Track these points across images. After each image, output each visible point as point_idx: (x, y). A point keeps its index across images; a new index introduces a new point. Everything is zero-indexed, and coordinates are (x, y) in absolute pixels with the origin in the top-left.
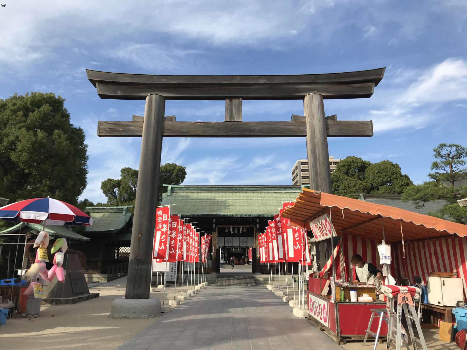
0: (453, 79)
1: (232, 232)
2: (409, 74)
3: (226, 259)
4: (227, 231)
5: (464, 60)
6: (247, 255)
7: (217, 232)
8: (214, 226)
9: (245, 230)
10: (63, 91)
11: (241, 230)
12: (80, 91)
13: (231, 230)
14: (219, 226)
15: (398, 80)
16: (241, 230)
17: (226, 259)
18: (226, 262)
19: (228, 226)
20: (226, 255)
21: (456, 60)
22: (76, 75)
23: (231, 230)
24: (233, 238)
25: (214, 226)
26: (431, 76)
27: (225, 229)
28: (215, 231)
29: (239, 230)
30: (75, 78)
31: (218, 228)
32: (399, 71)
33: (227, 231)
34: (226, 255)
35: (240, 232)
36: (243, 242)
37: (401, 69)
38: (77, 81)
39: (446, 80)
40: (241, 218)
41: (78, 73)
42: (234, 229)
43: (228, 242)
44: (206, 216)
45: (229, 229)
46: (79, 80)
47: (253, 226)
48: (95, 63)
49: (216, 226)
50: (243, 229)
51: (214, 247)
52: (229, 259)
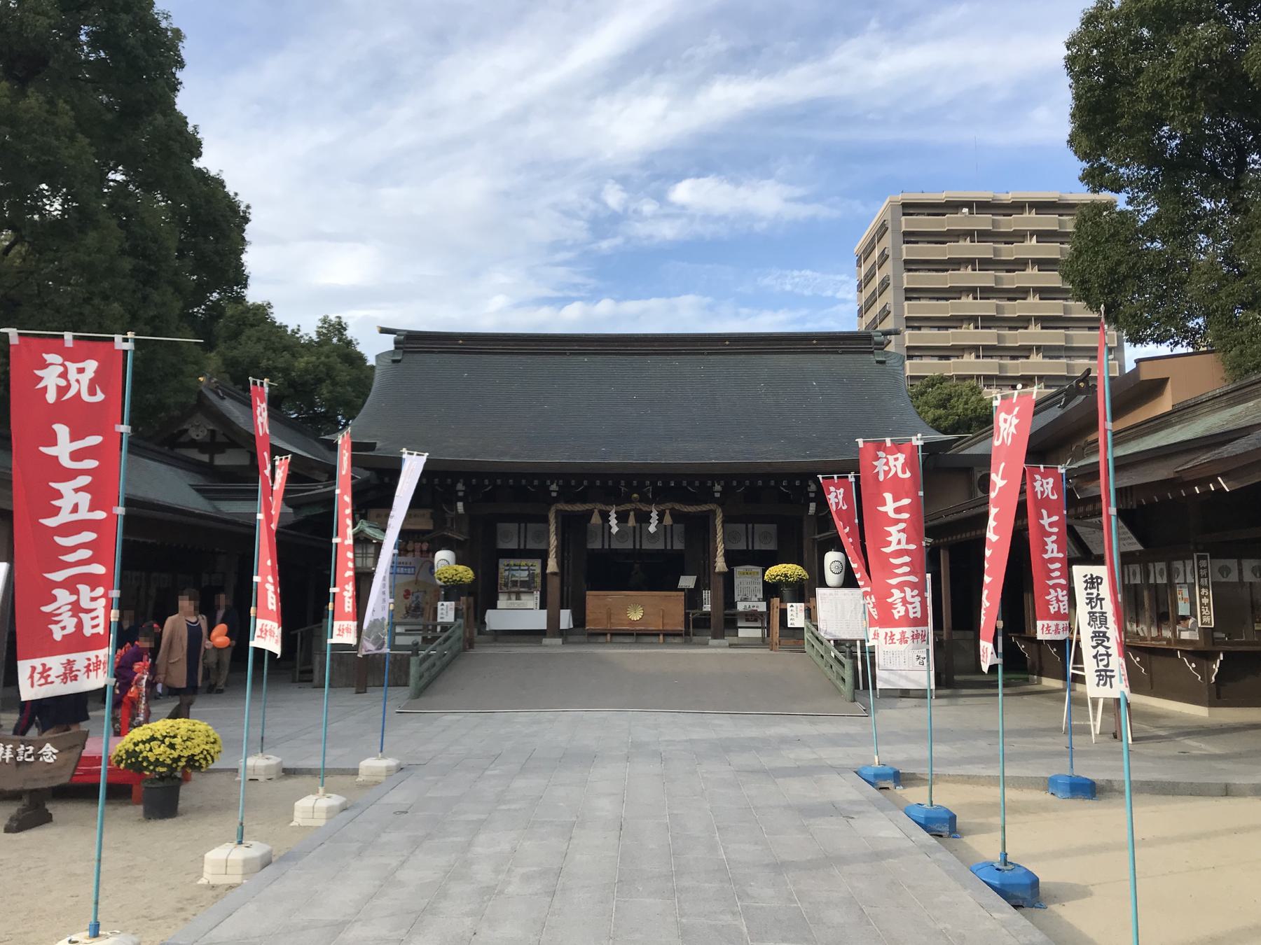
20: (552, 566)
34: (552, 566)
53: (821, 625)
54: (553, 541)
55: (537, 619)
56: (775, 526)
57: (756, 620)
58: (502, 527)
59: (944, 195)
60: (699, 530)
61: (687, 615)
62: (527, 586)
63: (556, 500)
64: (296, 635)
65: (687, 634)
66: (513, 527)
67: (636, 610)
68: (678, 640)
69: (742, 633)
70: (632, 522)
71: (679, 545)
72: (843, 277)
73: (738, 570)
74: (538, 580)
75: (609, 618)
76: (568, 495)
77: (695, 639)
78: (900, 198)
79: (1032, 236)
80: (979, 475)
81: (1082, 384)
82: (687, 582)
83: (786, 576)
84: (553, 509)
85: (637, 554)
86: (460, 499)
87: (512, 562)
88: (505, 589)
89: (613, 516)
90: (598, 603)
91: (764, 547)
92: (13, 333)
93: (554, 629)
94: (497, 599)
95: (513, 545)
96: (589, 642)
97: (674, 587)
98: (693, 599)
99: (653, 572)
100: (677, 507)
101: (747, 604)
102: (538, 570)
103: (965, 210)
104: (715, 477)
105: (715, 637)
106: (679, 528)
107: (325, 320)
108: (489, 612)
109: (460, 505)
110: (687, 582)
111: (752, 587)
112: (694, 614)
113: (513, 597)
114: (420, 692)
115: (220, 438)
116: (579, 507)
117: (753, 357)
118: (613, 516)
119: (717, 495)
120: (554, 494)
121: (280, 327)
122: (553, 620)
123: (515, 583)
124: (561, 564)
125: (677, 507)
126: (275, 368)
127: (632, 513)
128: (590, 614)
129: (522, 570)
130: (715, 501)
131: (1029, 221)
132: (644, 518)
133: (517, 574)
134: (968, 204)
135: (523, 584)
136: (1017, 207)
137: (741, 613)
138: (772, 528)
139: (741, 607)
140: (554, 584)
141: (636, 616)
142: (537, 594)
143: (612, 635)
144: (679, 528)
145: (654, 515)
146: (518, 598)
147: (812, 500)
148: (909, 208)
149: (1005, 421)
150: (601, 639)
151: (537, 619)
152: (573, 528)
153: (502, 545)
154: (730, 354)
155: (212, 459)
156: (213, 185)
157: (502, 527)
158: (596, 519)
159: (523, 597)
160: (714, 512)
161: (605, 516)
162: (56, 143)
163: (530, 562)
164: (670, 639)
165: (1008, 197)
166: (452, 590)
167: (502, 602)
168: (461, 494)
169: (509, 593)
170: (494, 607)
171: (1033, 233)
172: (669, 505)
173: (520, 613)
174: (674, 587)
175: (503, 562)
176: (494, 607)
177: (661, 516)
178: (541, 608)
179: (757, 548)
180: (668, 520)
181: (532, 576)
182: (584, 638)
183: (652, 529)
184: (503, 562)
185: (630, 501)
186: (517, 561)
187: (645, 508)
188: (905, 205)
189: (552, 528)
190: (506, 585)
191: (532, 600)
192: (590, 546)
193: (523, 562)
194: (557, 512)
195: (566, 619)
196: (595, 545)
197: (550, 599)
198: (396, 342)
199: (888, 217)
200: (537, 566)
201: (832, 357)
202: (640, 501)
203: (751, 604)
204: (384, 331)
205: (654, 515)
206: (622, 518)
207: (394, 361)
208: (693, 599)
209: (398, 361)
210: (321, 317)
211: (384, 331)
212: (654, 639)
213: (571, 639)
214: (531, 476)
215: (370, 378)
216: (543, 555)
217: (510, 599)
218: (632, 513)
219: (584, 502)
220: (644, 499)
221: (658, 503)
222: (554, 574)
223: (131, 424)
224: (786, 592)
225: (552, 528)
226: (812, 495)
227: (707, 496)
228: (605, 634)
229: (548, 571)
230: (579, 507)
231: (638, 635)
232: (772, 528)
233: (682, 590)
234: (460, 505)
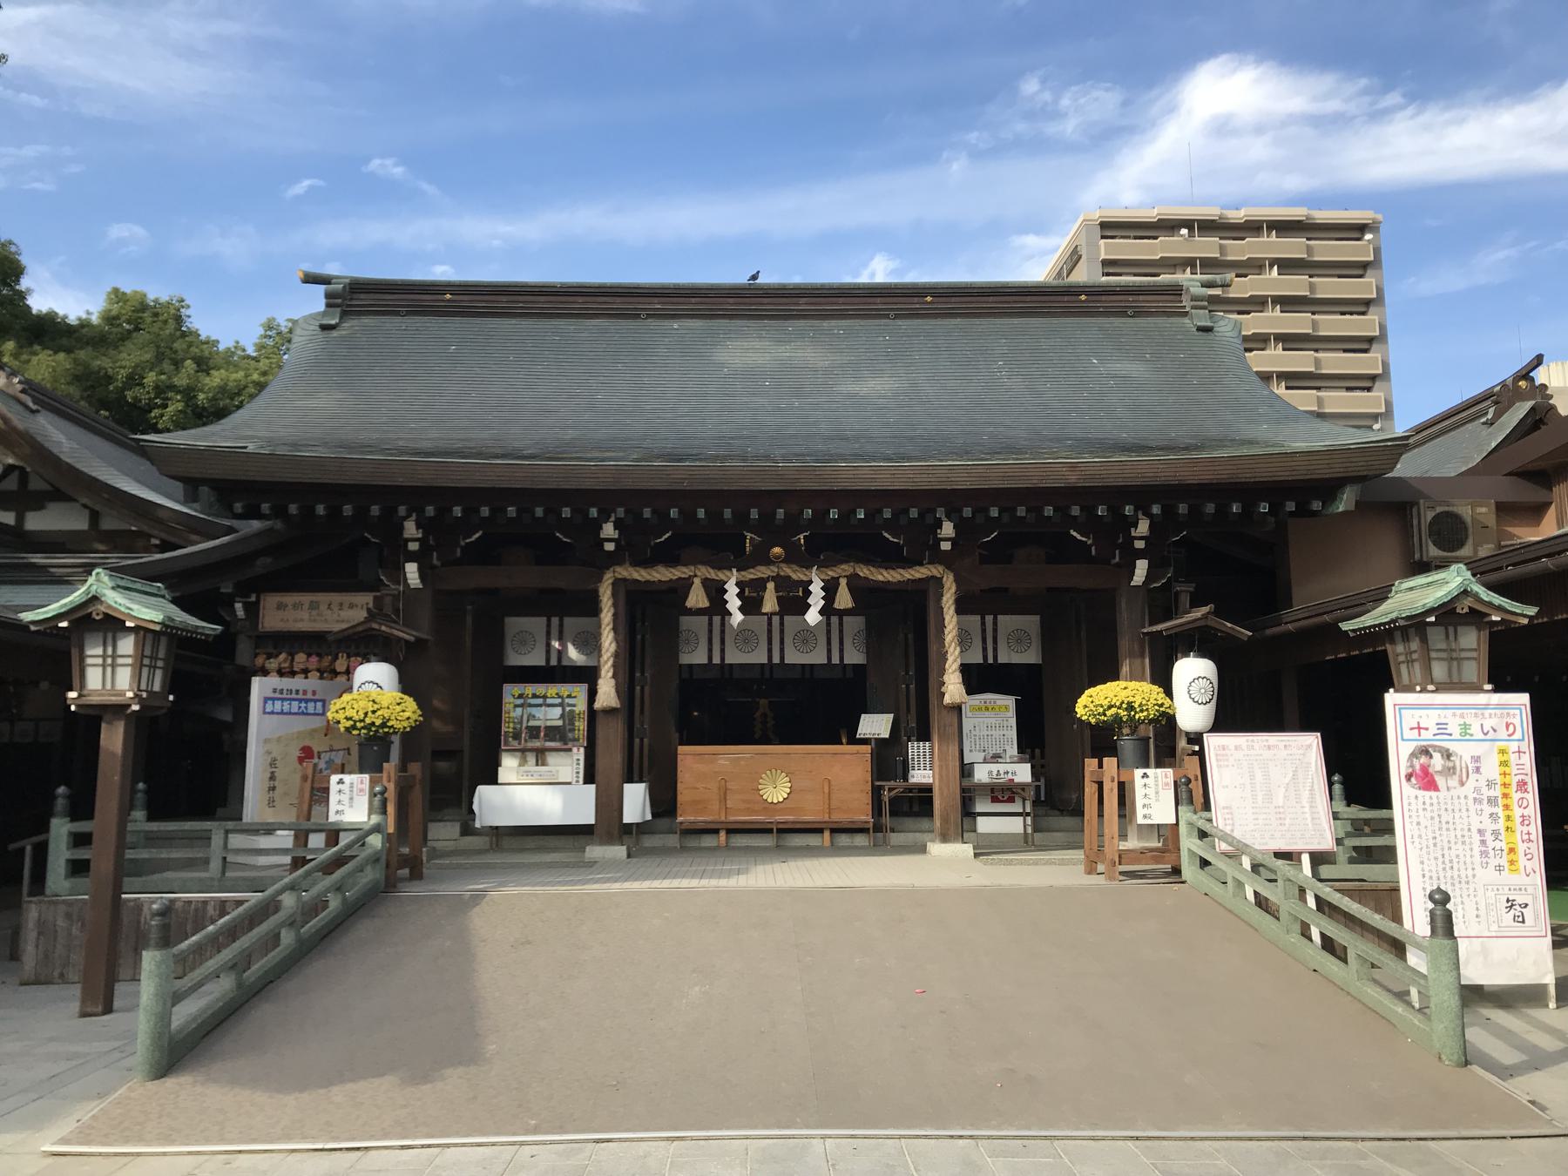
20: (607, 693)
53: (1220, 818)
54: (608, 642)
55: (579, 806)
56: (1037, 618)
57: (1011, 800)
58: (515, 624)
59: (1156, 212)
60: (899, 623)
61: (876, 792)
62: (559, 736)
63: (614, 559)
64: (23, 850)
65: (878, 828)
66: (536, 624)
67: (777, 778)
68: (860, 840)
69: (985, 825)
70: (770, 603)
73: (1485, 634)
74: (581, 725)
75: (724, 799)
76: (635, 549)
77: (896, 839)
78: (1097, 215)
79: (1271, 266)
80: (1430, 515)
81: (1522, 384)
82: (875, 725)
83: (1130, 707)
84: (608, 578)
85: (771, 678)
86: (412, 557)
87: (530, 689)
88: (515, 744)
89: (732, 592)
90: (705, 769)
91: (1017, 659)
93: (608, 825)
94: (497, 764)
95: (535, 659)
96: (683, 849)
98: (888, 759)
99: (805, 709)
100: (864, 571)
101: (994, 767)
102: (581, 705)
103: (1184, 231)
105: (945, 838)
107: (269, 326)
108: (482, 790)
109: (412, 569)
110: (875, 725)
111: (997, 733)
112: (891, 789)
113: (531, 758)
114: (176, 1054)
115: (36, 484)
116: (662, 574)
117: (977, 321)
118: (732, 592)
119: (946, 546)
120: (610, 547)
121: (207, 343)
122: (609, 805)
123: (534, 732)
124: (627, 689)
125: (864, 571)
126: (172, 387)
127: (771, 586)
128: (684, 795)
129: (551, 706)
130: (938, 557)
131: (1270, 245)
132: (795, 603)
133: (539, 713)
134: (1188, 224)
135: (553, 733)
136: (1253, 227)
137: (983, 786)
138: (1031, 622)
139: (982, 774)
140: (612, 736)
141: (776, 791)
142: (579, 754)
143: (730, 831)
145: (816, 588)
146: (541, 761)
147: (1141, 554)
148: (1110, 228)
150: (708, 841)
151: (579, 806)
152: (652, 618)
153: (515, 659)
154: (936, 316)
155: (20, 519)
157: (515, 624)
159: (552, 758)
160: (938, 581)
162: (241, 374)
163: (565, 689)
164: (844, 840)
165: (1238, 215)
166: (370, 748)
167: (509, 766)
168: (413, 546)
169: (523, 751)
170: (493, 780)
171: (1273, 262)
172: (847, 569)
173: (533, 791)
175: (511, 691)
176: (493, 780)
177: (830, 589)
178: (586, 782)
179: (1002, 660)
180: (844, 600)
181: (569, 717)
182: (673, 840)
183: (813, 617)
184: (511, 691)
185: (768, 562)
186: (540, 689)
187: (797, 574)
188: (1104, 225)
189: (607, 616)
190: (517, 736)
191: (568, 766)
192: (686, 659)
193: (552, 690)
194: (617, 583)
195: (635, 802)
196: (695, 656)
197: (601, 763)
198: (328, 296)
199: (1082, 242)
200: (580, 691)
201: (1117, 321)
202: (788, 560)
203: (1002, 767)
204: (311, 279)
205: (816, 588)
207: (324, 328)
208: (888, 759)
209: (332, 327)
210: (264, 320)
211: (311, 279)
212: (813, 840)
213: (649, 841)
215: (680, 730)
216: (588, 676)
217: (523, 762)
218: (771, 586)
219: (673, 561)
221: (823, 565)
222: (609, 712)
224: (1127, 744)
225: (607, 616)
226: (1140, 544)
227: (925, 549)
228: (716, 831)
229: (597, 705)
230: (662, 574)
231: (783, 834)
232: (1031, 622)
233: (865, 741)
234: (412, 569)
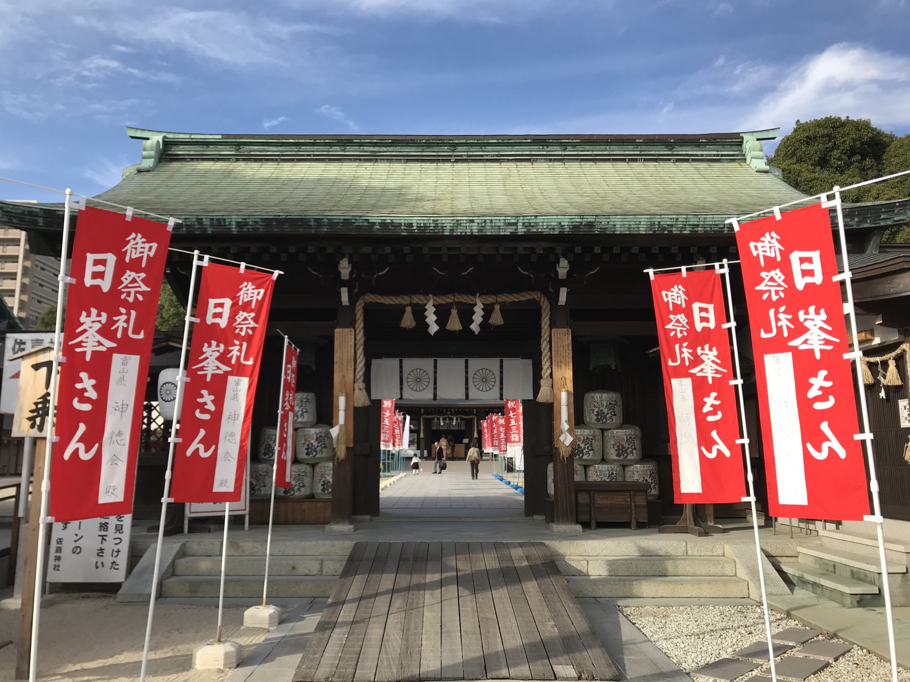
0: (848, 87)
1: (434, 328)
2: (759, 74)
3: (422, 444)
4: (408, 321)
5: (865, 48)
6: (476, 435)
7: (360, 324)
8: (345, 299)
9: (497, 319)
10: (61, 107)
11: (478, 318)
12: (97, 106)
13: (431, 318)
14: (371, 298)
15: (737, 88)
16: (478, 318)
17: (422, 444)
18: (422, 454)
19: (416, 299)
20: (422, 436)
21: (849, 48)
22: (86, 73)
23: (431, 318)
24: (440, 361)
25: (345, 299)
26: (802, 79)
27: (399, 312)
28: (352, 324)
29: (466, 315)
30: (83, 79)
31: (369, 311)
32: (738, 71)
33: (408, 321)
34: (422, 436)
35: (475, 327)
36: (485, 380)
37: (741, 66)
38: (88, 86)
39: (830, 88)
40: (482, 239)
41: (89, 70)
42: (442, 315)
43: (418, 380)
44: (287, 229)
45: (419, 313)
46: (94, 85)
47: (535, 295)
48: (121, 48)
49: (353, 299)
50: (488, 311)
51: (342, 401)
52: (429, 448)
71: (463, 428)
72: (394, 670)
82: (466, 441)
92: (651, 271)
97: (461, 443)
104: (473, 408)
106: (463, 422)
116: (430, 417)
144: (463, 422)
149: (756, 248)
156: (789, 260)
158: (436, 420)
161: (439, 419)
174: (461, 443)
196: (434, 428)
206: (444, 419)
214: (416, 408)
220: (452, 414)
223: (831, 189)
227: (472, 413)
230: (430, 417)
